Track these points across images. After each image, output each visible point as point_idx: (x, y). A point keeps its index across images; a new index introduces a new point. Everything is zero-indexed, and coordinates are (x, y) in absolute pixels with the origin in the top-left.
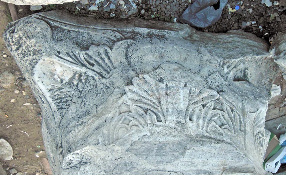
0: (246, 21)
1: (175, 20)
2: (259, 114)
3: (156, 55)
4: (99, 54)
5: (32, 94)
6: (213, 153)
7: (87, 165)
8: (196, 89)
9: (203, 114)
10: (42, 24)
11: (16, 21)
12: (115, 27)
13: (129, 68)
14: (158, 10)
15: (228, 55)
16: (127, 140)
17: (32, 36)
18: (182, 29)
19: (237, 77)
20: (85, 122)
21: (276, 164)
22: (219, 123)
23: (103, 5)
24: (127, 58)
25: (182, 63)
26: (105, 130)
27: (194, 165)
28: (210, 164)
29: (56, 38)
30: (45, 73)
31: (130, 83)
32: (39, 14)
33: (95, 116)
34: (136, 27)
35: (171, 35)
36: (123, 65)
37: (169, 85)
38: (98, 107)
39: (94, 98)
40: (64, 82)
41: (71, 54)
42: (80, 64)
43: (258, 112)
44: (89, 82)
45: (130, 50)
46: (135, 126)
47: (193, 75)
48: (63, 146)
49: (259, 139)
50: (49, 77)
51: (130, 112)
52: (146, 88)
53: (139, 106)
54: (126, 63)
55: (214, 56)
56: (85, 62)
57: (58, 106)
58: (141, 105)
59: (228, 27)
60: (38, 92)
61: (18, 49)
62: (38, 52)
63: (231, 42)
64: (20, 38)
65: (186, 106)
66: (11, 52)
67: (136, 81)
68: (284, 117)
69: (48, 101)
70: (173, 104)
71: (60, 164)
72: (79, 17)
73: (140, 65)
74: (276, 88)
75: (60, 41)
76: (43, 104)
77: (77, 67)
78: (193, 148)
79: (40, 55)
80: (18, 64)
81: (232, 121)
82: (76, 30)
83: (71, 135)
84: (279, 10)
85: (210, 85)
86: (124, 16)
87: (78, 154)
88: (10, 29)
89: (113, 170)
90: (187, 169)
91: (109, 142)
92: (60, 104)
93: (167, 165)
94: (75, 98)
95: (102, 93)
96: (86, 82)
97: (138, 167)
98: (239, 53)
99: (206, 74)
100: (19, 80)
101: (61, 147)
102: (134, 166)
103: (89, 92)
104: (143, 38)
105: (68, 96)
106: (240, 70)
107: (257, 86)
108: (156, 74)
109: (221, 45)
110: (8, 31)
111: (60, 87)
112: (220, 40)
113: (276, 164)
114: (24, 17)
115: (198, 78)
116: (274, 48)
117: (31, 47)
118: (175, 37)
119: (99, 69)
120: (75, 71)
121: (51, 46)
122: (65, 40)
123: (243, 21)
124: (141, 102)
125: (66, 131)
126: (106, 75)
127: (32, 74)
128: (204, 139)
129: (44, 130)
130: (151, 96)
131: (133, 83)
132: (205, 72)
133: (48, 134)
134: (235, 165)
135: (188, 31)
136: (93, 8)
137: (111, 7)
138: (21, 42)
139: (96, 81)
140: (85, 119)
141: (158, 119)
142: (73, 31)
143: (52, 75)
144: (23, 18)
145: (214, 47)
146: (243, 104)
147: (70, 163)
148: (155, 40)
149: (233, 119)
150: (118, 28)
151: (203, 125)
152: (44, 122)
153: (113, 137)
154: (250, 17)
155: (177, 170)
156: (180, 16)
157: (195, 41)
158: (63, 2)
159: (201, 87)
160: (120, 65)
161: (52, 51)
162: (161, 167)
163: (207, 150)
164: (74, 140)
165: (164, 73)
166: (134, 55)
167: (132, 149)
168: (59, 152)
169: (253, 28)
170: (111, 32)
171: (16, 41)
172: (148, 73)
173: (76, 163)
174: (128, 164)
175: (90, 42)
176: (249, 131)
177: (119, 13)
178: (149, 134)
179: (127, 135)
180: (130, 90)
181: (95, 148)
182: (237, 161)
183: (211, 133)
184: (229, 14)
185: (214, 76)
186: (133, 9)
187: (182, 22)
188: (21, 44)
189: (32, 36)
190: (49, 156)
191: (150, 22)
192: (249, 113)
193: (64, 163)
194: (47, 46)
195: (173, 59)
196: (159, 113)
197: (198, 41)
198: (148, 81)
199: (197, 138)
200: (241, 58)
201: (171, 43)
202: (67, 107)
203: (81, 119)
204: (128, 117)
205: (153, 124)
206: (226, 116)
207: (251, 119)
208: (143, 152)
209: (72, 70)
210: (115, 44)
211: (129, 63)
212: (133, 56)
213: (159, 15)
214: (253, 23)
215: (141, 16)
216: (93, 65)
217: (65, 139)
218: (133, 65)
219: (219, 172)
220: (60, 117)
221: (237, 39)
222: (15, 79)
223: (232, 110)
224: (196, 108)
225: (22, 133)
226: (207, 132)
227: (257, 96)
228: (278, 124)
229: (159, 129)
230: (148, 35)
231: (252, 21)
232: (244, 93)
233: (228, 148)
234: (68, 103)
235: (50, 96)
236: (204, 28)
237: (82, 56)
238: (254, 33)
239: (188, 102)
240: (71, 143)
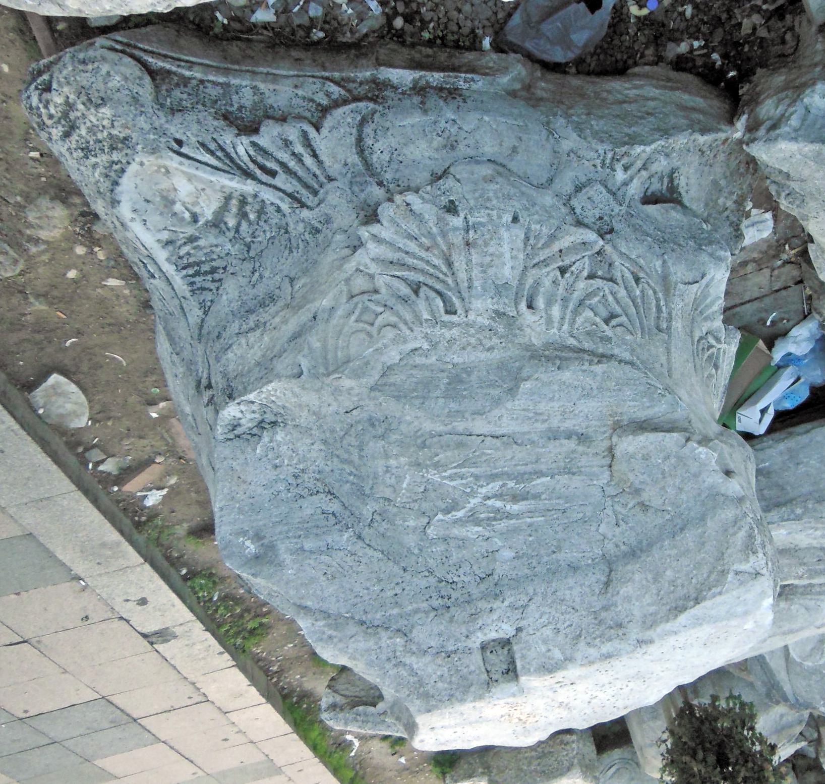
0: (677, 41)
1: (487, 43)
2: (707, 286)
3: (438, 141)
4: (287, 143)
5: (121, 255)
6: (588, 386)
7: (278, 429)
8: (544, 228)
9: (561, 291)
10: (126, 66)
11: (51, 59)
12: (324, 69)
13: (368, 179)
14: (441, 16)
15: (628, 135)
16: (372, 363)
17: (102, 99)
18: (505, 70)
19: (653, 193)
20: (265, 323)
21: (763, 411)
22: (605, 314)
23: (290, 7)
24: (361, 151)
25: (505, 162)
26: (314, 341)
27: (541, 417)
28: (581, 414)
29: (168, 104)
30: (148, 198)
31: (371, 217)
32: (111, 35)
33: (287, 306)
34: (382, 68)
35: (474, 86)
36: (352, 170)
37: (471, 220)
38: (295, 283)
39: (283, 260)
40: (201, 222)
41: (213, 146)
42: (238, 172)
43: (704, 282)
44: (266, 218)
45: (368, 130)
46: (389, 327)
47: (532, 192)
48: (213, 384)
49: (708, 350)
50: (161, 208)
51: (376, 291)
52: (414, 229)
53: (398, 277)
54: (361, 167)
55: (590, 139)
56: (252, 166)
57: (192, 284)
58: (404, 273)
59: (629, 58)
60: (136, 249)
61: (67, 135)
62: (124, 144)
63: (635, 101)
64: (69, 106)
65: (518, 272)
66: (49, 145)
67: (386, 211)
68: (784, 293)
69: (164, 270)
70: (484, 267)
71: (209, 428)
72: (225, 43)
73: (397, 170)
74: (760, 219)
75: (180, 111)
76: (152, 281)
77: (231, 180)
78: (536, 376)
79: (129, 151)
80: (73, 177)
81: (636, 306)
82: (221, 80)
83: (230, 355)
84: (764, 7)
85: (580, 217)
86: (348, 38)
87: (253, 402)
88: (38, 82)
89: (342, 438)
90: (526, 428)
91: (327, 369)
92: (197, 279)
93: (473, 419)
94: (234, 262)
95: (301, 245)
96: (259, 218)
97: (403, 428)
98: (654, 129)
99: (569, 188)
100: (83, 219)
101: (209, 386)
102: (394, 426)
103: (270, 244)
104: (401, 96)
105: (215, 257)
106: (659, 174)
107: (705, 214)
108: (439, 193)
109: (608, 108)
110: (33, 87)
111: (191, 236)
112: (605, 95)
113: (763, 411)
114: (73, 44)
115: (548, 199)
116: (744, 113)
117: (101, 128)
118: (486, 92)
119: (289, 185)
120: (228, 191)
121: (157, 124)
122: (193, 108)
123: (670, 39)
124: (403, 265)
125: (218, 346)
126: (310, 200)
127: (115, 203)
128: (563, 354)
129: (163, 347)
130: (427, 249)
131: (381, 217)
132: (565, 184)
133: (174, 355)
134: (642, 415)
135: (519, 74)
136: (263, 16)
137: (312, 13)
138: (72, 116)
139: (284, 215)
140: (264, 316)
141: (449, 308)
142: (213, 83)
143: (168, 202)
144: (71, 49)
145: (588, 114)
146: (664, 262)
147: (236, 426)
148: (433, 100)
149: (639, 300)
150: (333, 70)
151: (563, 318)
152: (160, 328)
153: (336, 356)
154: (688, 27)
155: (500, 432)
156: (499, 29)
157: (541, 99)
158: (169, 6)
159: (555, 222)
160: (344, 171)
161: (161, 139)
162: (460, 426)
163: (571, 381)
164: (240, 367)
165: (460, 190)
166: (380, 143)
167: (385, 385)
168: (206, 400)
169: (697, 59)
170: (314, 83)
171: (60, 114)
172: (417, 191)
173: (250, 425)
174: (379, 420)
175: (260, 113)
176: (680, 330)
177: (336, 29)
178: (426, 346)
179: (371, 350)
180: (375, 238)
181: (294, 385)
182: (648, 404)
183: (581, 337)
184: (630, 21)
185: (590, 191)
186: (373, 17)
187: (506, 48)
188: (75, 121)
189: (102, 99)
190: (182, 411)
191: (420, 52)
192: (681, 286)
193: (218, 427)
194: (147, 127)
195: (480, 150)
196: (449, 293)
197: (548, 100)
198: (418, 212)
199: (547, 353)
200: (659, 143)
201: (476, 109)
202: (217, 284)
203: (254, 315)
204: (372, 306)
205: (434, 321)
206: (622, 293)
207: (687, 301)
208: (414, 390)
209: (218, 188)
210: (328, 116)
211: (368, 165)
212: (378, 146)
213: (442, 31)
214: (696, 44)
215: (394, 35)
216: (273, 174)
217: (217, 368)
218: (379, 170)
219: (605, 432)
220: (200, 313)
221: (652, 91)
222: (72, 215)
223: (637, 280)
224: (543, 278)
225: (107, 357)
226: (572, 336)
227: (701, 242)
228: (768, 312)
229: (452, 332)
230: (413, 88)
231: (692, 40)
232: (669, 233)
233: (624, 373)
234: (217, 276)
235: (168, 260)
236: (567, 64)
237: (241, 150)
238: (698, 74)
239: (522, 261)
240: (232, 375)
